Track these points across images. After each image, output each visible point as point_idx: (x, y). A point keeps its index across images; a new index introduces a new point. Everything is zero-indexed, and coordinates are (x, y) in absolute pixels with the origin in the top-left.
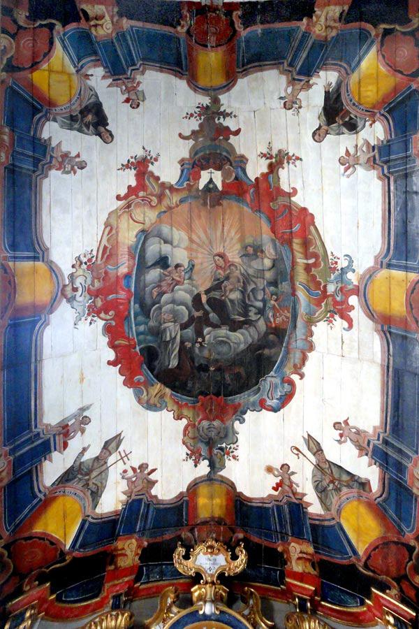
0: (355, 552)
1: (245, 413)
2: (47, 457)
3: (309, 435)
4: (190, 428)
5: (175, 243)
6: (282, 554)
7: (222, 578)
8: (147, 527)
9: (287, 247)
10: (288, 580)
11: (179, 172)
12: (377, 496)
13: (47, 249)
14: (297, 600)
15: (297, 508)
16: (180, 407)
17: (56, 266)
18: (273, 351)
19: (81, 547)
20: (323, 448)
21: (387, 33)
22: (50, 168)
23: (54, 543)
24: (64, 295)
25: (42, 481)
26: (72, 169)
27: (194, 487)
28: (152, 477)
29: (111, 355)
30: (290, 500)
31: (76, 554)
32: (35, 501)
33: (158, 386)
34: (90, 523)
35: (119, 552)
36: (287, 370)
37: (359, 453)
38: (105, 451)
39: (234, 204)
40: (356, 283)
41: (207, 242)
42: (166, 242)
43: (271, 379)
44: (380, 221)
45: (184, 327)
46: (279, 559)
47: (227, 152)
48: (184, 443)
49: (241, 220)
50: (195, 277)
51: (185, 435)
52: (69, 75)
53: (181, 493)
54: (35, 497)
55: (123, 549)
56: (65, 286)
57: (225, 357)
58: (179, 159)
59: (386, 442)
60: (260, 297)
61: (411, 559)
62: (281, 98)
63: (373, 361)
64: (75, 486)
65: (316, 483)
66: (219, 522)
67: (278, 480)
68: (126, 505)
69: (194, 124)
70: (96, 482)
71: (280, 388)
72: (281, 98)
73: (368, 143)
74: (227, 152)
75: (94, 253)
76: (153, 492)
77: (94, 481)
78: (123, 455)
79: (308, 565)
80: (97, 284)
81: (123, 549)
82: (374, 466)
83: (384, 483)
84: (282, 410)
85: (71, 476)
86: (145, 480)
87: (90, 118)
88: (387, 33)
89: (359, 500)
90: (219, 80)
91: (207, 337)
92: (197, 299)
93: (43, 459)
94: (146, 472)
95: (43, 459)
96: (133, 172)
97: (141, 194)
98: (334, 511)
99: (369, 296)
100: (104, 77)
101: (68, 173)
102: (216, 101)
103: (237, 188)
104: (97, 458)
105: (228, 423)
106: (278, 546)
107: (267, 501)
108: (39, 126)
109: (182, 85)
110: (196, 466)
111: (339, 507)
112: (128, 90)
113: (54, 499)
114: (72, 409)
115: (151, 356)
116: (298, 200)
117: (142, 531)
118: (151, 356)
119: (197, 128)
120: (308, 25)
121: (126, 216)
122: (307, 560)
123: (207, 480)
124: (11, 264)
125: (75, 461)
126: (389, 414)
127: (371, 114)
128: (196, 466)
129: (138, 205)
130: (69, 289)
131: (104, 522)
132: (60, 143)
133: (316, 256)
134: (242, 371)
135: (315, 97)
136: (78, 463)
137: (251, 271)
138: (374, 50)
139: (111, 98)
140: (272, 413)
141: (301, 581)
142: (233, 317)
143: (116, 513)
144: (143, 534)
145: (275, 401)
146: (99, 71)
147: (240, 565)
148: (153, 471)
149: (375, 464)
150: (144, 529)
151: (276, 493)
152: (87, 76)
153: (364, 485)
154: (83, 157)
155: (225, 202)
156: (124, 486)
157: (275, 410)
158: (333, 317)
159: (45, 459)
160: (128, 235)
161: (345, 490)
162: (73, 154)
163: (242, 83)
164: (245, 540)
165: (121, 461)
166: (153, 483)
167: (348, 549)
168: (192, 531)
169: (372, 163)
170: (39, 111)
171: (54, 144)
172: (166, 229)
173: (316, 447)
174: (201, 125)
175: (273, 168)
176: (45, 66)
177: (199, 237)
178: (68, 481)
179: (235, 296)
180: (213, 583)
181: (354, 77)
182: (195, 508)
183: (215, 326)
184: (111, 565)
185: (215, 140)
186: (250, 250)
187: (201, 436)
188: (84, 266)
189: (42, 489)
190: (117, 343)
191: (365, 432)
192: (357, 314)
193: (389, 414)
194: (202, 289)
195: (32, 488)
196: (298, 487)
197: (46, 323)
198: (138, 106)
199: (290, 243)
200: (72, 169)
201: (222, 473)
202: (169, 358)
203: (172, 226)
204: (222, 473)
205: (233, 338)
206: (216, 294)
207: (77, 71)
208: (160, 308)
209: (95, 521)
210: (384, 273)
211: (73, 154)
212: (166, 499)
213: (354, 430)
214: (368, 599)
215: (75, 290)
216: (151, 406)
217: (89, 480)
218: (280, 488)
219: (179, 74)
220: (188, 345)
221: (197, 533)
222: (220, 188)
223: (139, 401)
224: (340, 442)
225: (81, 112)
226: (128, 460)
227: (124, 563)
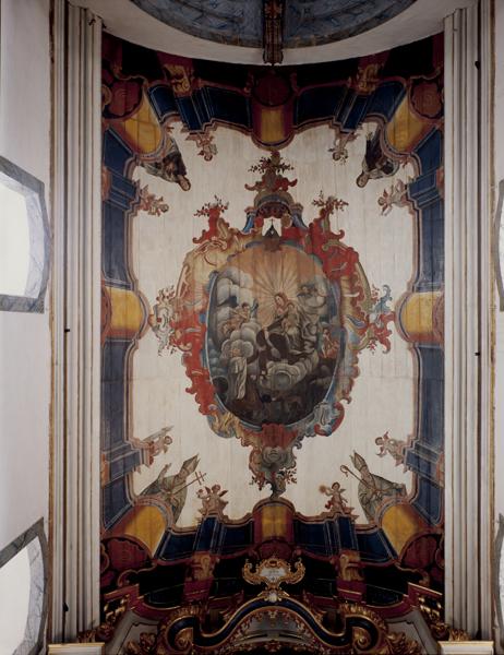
5: (242, 284)
6: (333, 566)
8: (220, 544)
9: (336, 284)
11: (245, 220)
13: (137, 281)
15: (346, 521)
16: (247, 434)
17: (145, 298)
18: (325, 380)
19: (165, 555)
21: (416, 83)
22: (139, 208)
24: (150, 324)
26: (157, 211)
27: (259, 508)
28: (223, 498)
29: (189, 384)
32: (127, 506)
33: (229, 414)
34: (172, 536)
36: (337, 397)
39: (292, 248)
40: (393, 310)
41: (268, 283)
42: (234, 283)
43: (325, 405)
44: (411, 250)
45: (250, 361)
46: (333, 571)
47: (286, 201)
48: (250, 468)
49: (298, 262)
50: (259, 315)
51: (251, 460)
52: (154, 126)
53: (248, 514)
54: (127, 502)
55: (199, 563)
56: (151, 315)
57: (286, 388)
58: (245, 208)
59: (418, 447)
60: (314, 332)
62: (331, 150)
63: (407, 377)
64: (160, 498)
66: (282, 540)
67: (329, 498)
69: (258, 177)
71: (331, 414)
72: (331, 150)
73: (401, 183)
74: (286, 201)
75: (175, 288)
76: (225, 512)
79: (356, 572)
80: (177, 318)
85: (156, 489)
87: (171, 166)
88: (416, 83)
90: (278, 136)
91: (270, 371)
92: (260, 335)
94: (218, 493)
96: (207, 218)
97: (214, 238)
98: (376, 520)
99: (403, 320)
100: (183, 131)
101: (153, 214)
102: (276, 155)
103: (294, 233)
105: (288, 449)
108: (130, 170)
109: (247, 140)
112: (203, 144)
113: (143, 507)
114: (157, 429)
115: (222, 387)
116: (346, 241)
117: (215, 549)
118: (222, 387)
119: (260, 180)
120: (353, 83)
121: (200, 259)
122: (354, 568)
124: (108, 288)
127: (404, 156)
129: (211, 248)
130: (154, 319)
132: (146, 187)
133: (360, 289)
134: (297, 399)
135: (358, 148)
137: (306, 309)
138: (405, 100)
139: (189, 150)
140: (324, 437)
141: (351, 589)
142: (291, 351)
145: (327, 426)
146: (178, 126)
148: (224, 492)
150: (217, 546)
151: (329, 511)
152: (169, 129)
153: (400, 490)
154: (165, 202)
155: (284, 247)
156: (200, 504)
157: (327, 434)
158: (374, 343)
160: (203, 275)
161: (385, 498)
162: (157, 198)
163: (298, 138)
164: (302, 555)
166: (224, 504)
167: (389, 552)
169: (406, 200)
170: (129, 155)
171: (142, 187)
172: (234, 272)
174: (263, 177)
175: (325, 213)
176: (135, 116)
177: (263, 280)
178: (153, 493)
179: (293, 331)
181: (390, 126)
183: (276, 360)
185: (274, 191)
186: (305, 290)
188: (166, 300)
190: (193, 372)
191: (401, 442)
192: (395, 338)
194: (265, 326)
197: (135, 347)
198: (211, 158)
199: (338, 280)
200: (157, 211)
201: (283, 496)
202: (238, 387)
203: (239, 268)
204: (283, 496)
205: (291, 370)
206: (276, 331)
207: (162, 123)
208: (230, 343)
210: (415, 295)
211: (157, 198)
215: (159, 320)
216: (222, 433)
219: (245, 131)
220: (254, 377)
222: (280, 234)
223: (212, 427)
225: (164, 160)
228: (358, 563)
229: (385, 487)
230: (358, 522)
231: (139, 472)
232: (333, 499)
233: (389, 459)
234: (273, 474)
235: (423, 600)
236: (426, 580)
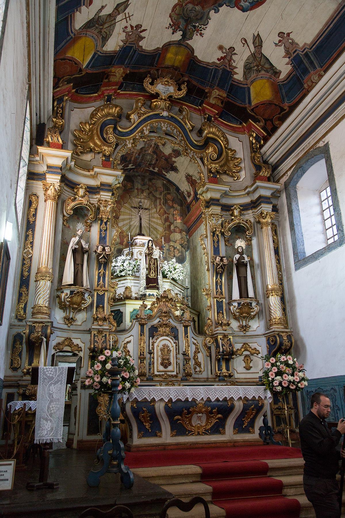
0: (250, 102)
1: (221, 6)
2: (79, 9)
3: (258, 34)
4: (178, 7)
7: (170, 98)
10: (204, 105)
12: (281, 81)
14: (207, 115)
20: (263, 45)
23: (76, 63)
25: (74, 26)
27: (167, 46)
28: (142, 34)
30: (226, 68)
31: (89, 71)
32: (69, 38)
34: (99, 56)
35: (112, 74)
37: (285, 55)
38: (116, 11)
48: (170, 16)
51: (173, 11)
53: (158, 48)
54: (68, 35)
55: (115, 72)
59: (306, 55)
61: (279, 114)
64: (93, 32)
65: (247, 64)
66: (176, 69)
67: (223, 55)
68: (122, 48)
70: (106, 31)
76: (141, 44)
77: (105, 30)
78: (127, 16)
81: (115, 72)
82: (289, 66)
83: (290, 76)
84: (248, 12)
86: (137, 35)
89: (268, 80)
93: (75, 10)
94: (139, 30)
95: (75, 10)
98: (249, 81)
104: (110, 15)
105: (207, 10)
106: (206, 89)
107: (210, 65)
110: (173, 33)
111: (254, 80)
113: (80, 38)
123: (178, 44)
125: (96, 14)
126: (321, 39)
128: (173, 33)
131: (106, 56)
136: (97, 17)
143: (115, 52)
144: (128, 67)
147: (182, 94)
149: (291, 65)
151: (218, 62)
153: (277, 73)
156: (123, 36)
157: (244, 10)
159: (77, 11)
161: (263, 72)
165: (125, 19)
166: (142, 38)
168: (158, 70)
173: (258, 41)
178: (89, 27)
180: (165, 100)
182: (164, 58)
184: (106, 79)
187: (184, 14)
189: (73, 31)
191: (297, 44)
193: (321, 39)
195: (67, 29)
196: (235, 62)
201: (189, 42)
204: (189, 42)
209: (101, 54)
212: (148, 49)
213: (290, 41)
214: (244, 123)
217: (102, 29)
218: (222, 60)
221: (160, 72)
224: (276, 45)
226: (130, 20)
227: (113, 79)
228: (224, 98)
229: (267, 66)
230: (235, 76)
231: (80, 12)
232: (225, 57)
233: (281, 51)
234: (187, 26)
235: (254, 135)
236: (262, 124)
